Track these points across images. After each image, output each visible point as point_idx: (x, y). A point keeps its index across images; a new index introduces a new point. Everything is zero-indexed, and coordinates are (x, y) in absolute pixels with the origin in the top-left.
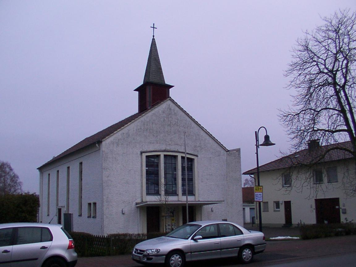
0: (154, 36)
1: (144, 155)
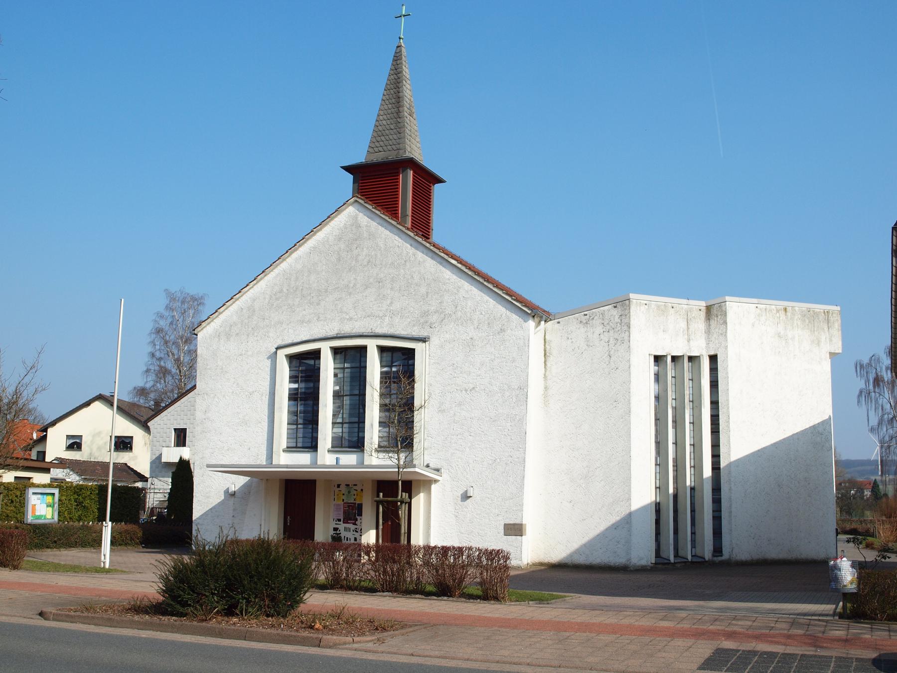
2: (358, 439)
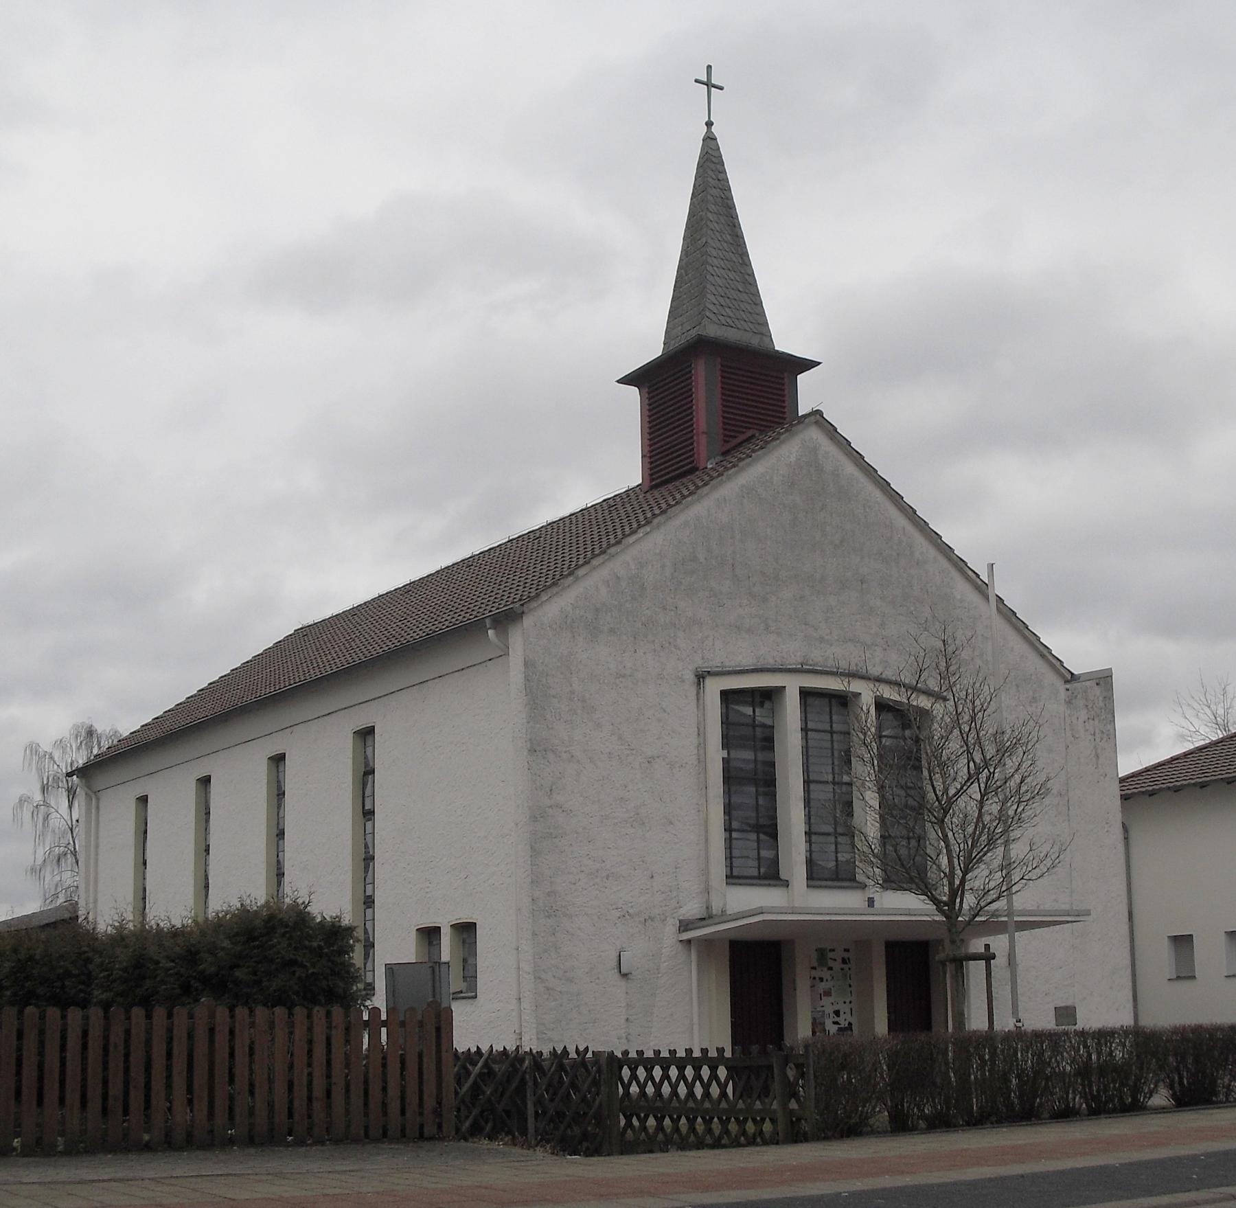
0: (709, 124)
1: (714, 687)
2: (837, 865)
